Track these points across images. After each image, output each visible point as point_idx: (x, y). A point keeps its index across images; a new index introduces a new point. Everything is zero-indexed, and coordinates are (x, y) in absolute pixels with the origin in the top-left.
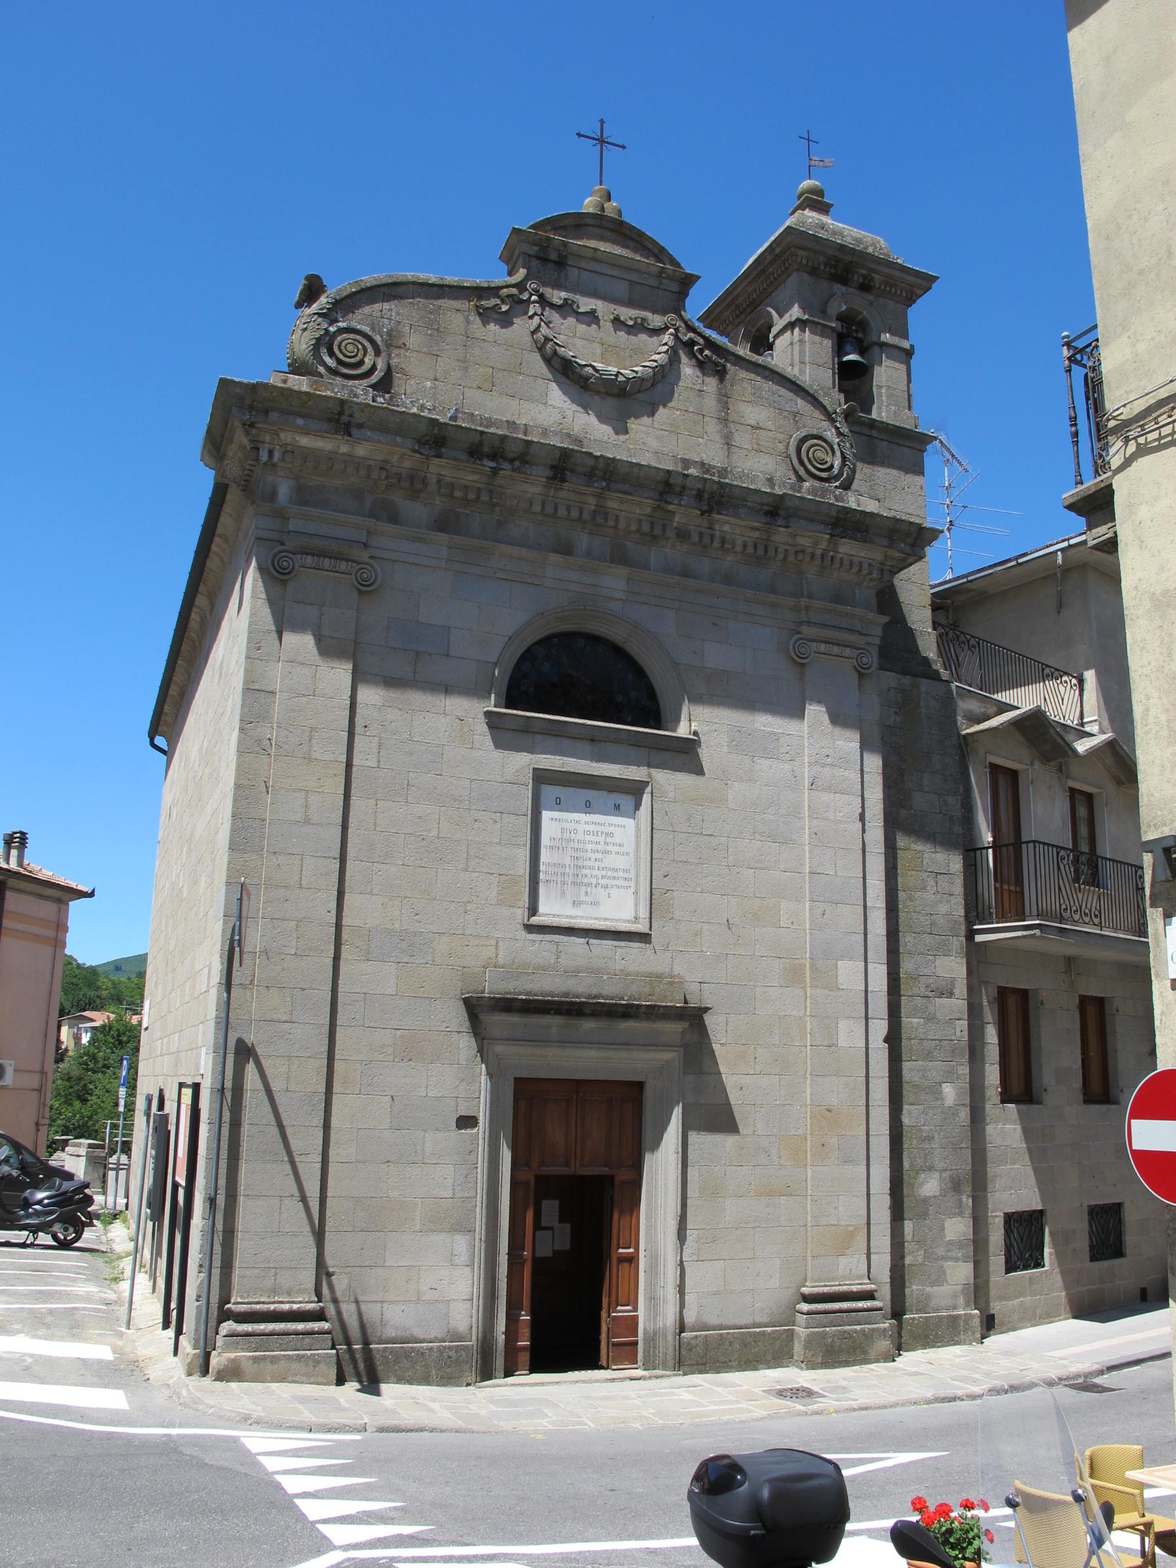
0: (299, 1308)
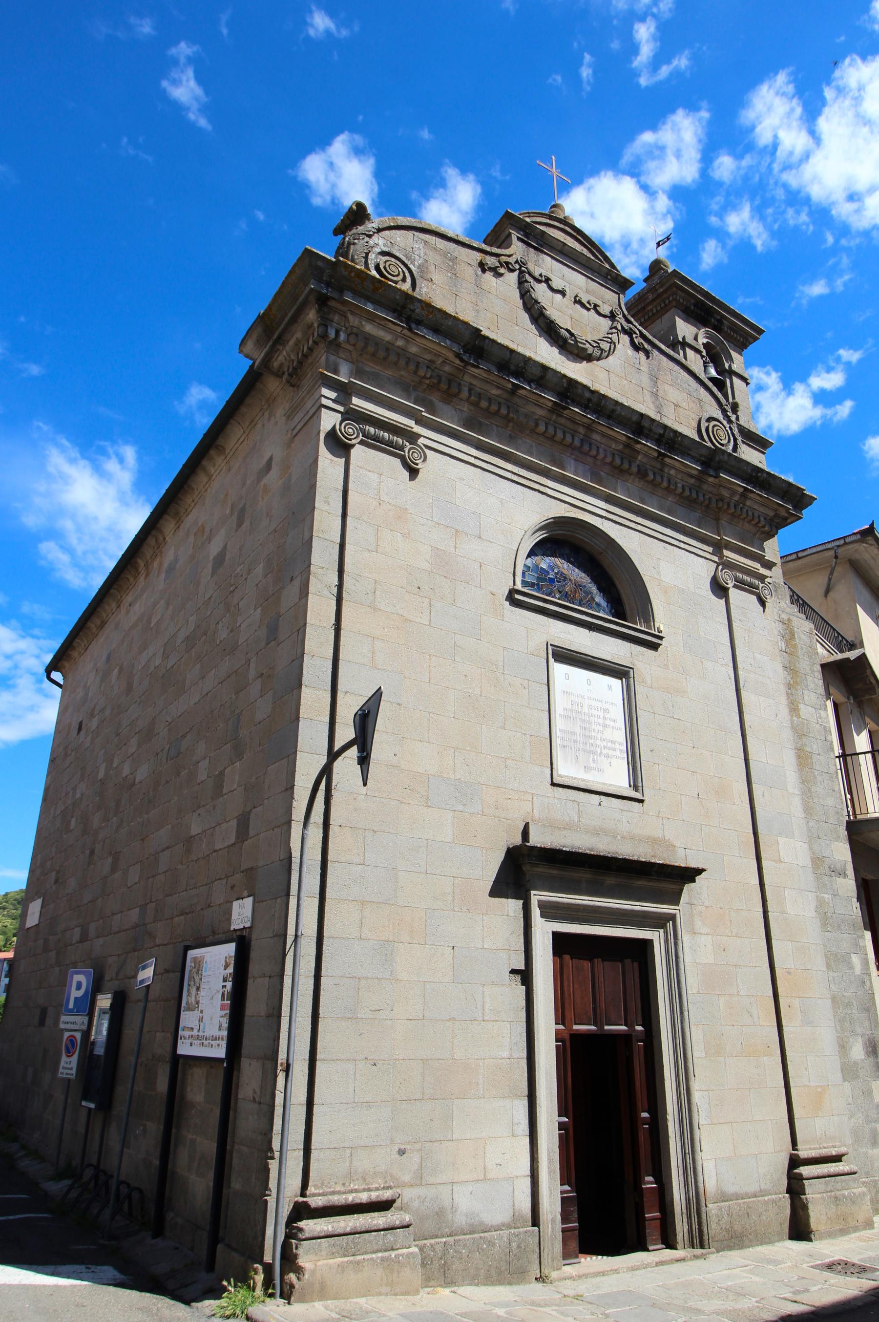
0: (377, 1196)
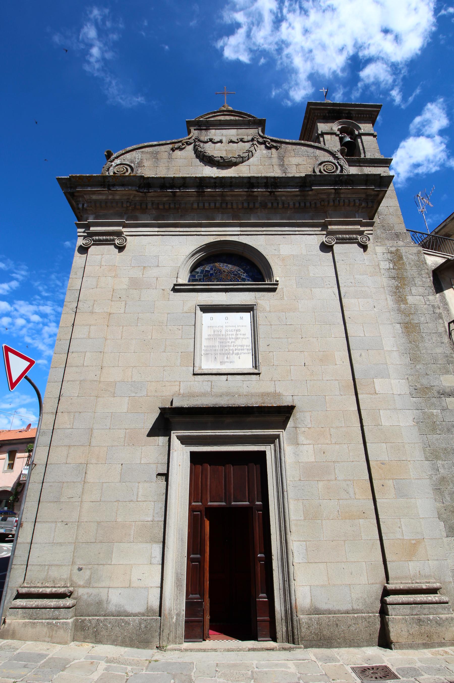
0: (56, 591)
